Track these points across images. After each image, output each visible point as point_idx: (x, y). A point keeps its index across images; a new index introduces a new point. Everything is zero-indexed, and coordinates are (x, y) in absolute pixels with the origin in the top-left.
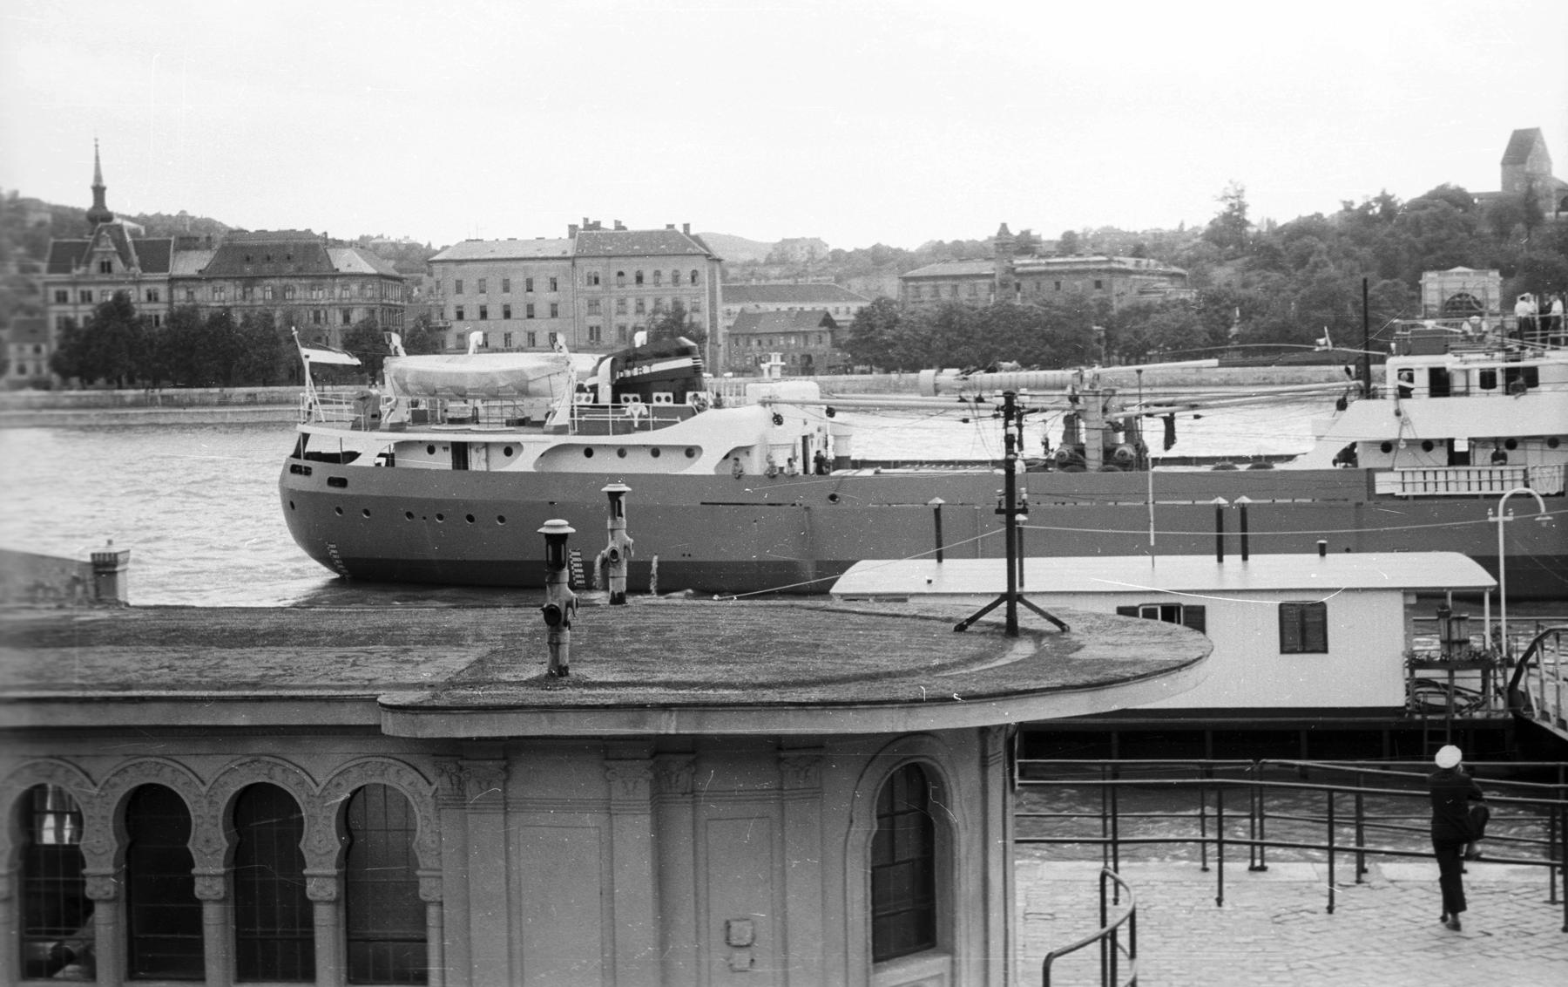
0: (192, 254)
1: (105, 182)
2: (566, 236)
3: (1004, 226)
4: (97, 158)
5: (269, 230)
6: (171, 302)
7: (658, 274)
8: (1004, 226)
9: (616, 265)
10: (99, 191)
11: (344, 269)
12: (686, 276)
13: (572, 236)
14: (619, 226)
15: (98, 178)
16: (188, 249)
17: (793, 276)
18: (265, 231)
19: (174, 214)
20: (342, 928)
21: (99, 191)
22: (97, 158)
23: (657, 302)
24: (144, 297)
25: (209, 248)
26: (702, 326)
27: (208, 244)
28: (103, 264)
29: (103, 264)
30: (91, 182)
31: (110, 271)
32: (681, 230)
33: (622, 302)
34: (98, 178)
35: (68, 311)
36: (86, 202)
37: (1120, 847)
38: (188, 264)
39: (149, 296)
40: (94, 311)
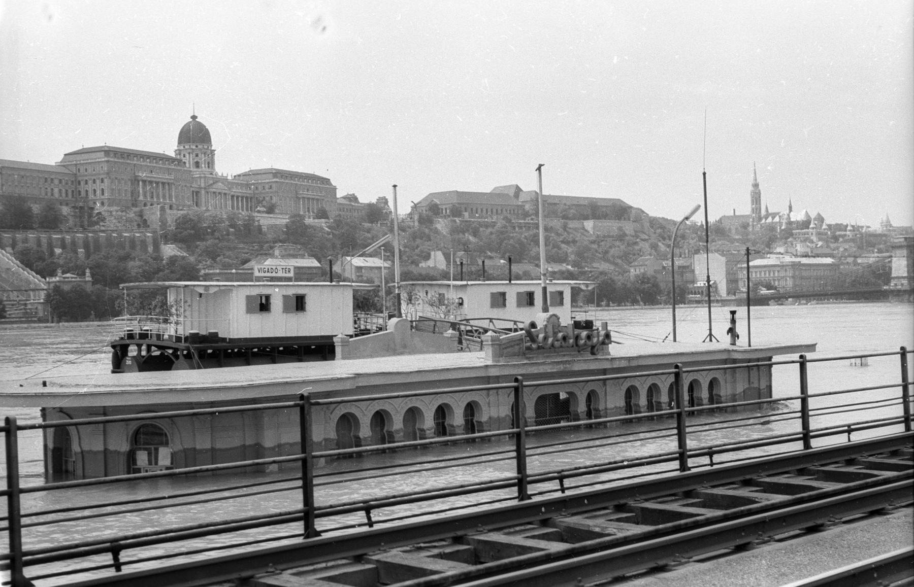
10: (756, 198)
21: (756, 198)
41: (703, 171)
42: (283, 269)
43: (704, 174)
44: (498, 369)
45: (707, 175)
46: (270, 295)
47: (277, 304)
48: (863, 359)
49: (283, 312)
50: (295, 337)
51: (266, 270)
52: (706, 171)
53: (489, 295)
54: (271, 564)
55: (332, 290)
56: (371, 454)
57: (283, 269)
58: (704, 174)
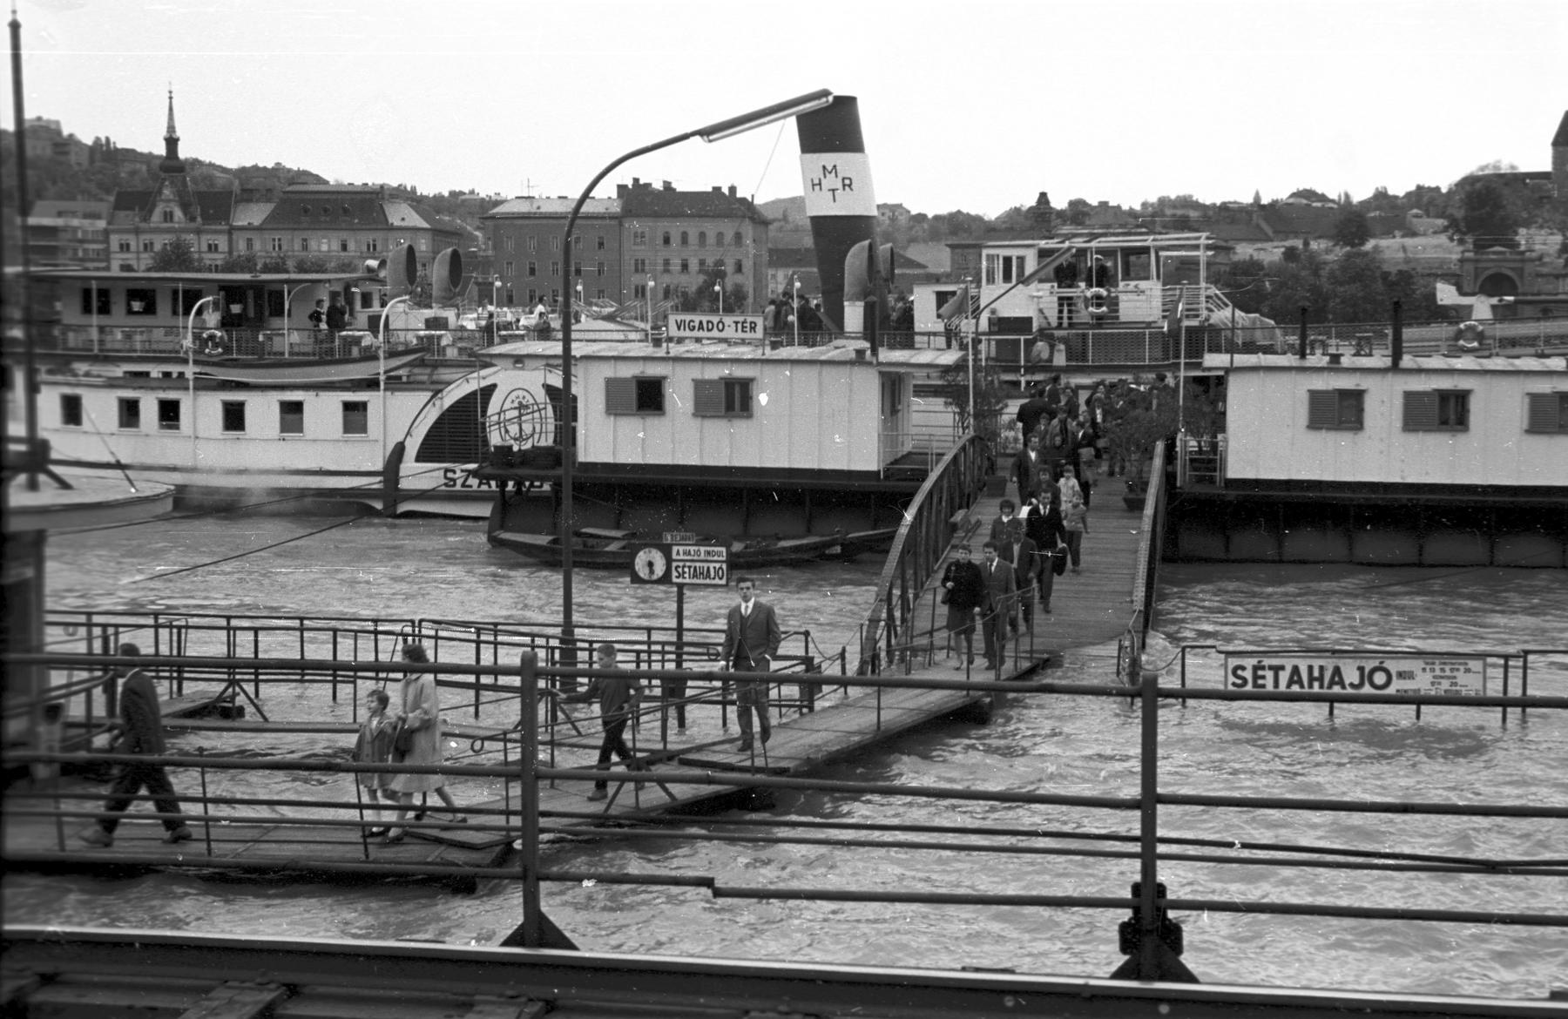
0: (254, 207)
1: (179, 133)
2: (614, 195)
3: (1043, 196)
4: (171, 109)
5: (139, 150)
6: (230, 252)
7: (702, 235)
8: (1043, 196)
9: (663, 225)
10: (172, 142)
11: (397, 223)
12: (729, 236)
13: (620, 195)
14: (667, 185)
15: (171, 128)
16: (249, 201)
17: (373, 620)
18: (133, 151)
19: (270, 166)
20: (600, 574)
21: (172, 142)
22: (171, 109)
23: (702, 263)
24: (204, 248)
25: (269, 201)
26: (745, 289)
27: (266, 195)
28: (165, 213)
29: (165, 213)
30: (164, 132)
31: (172, 220)
32: (726, 191)
33: (667, 263)
34: (171, 128)
35: (130, 258)
36: (160, 150)
37: (1133, 791)
38: (252, 215)
39: (121, 246)
40: (153, 258)
41: (9, 18)
42: (736, 323)
43: (15, 27)
44: (265, 708)
45: (23, 33)
46: (665, 378)
47: (679, 396)
48: (1520, 671)
49: (695, 415)
50: (726, 467)
51: (697, 324)
52: (20, 18)
53: (1305, 398)
54: (786, 998)
55: (820, 374)
56: (394, 883)
57: (736, 323)
58: (15, 27)
